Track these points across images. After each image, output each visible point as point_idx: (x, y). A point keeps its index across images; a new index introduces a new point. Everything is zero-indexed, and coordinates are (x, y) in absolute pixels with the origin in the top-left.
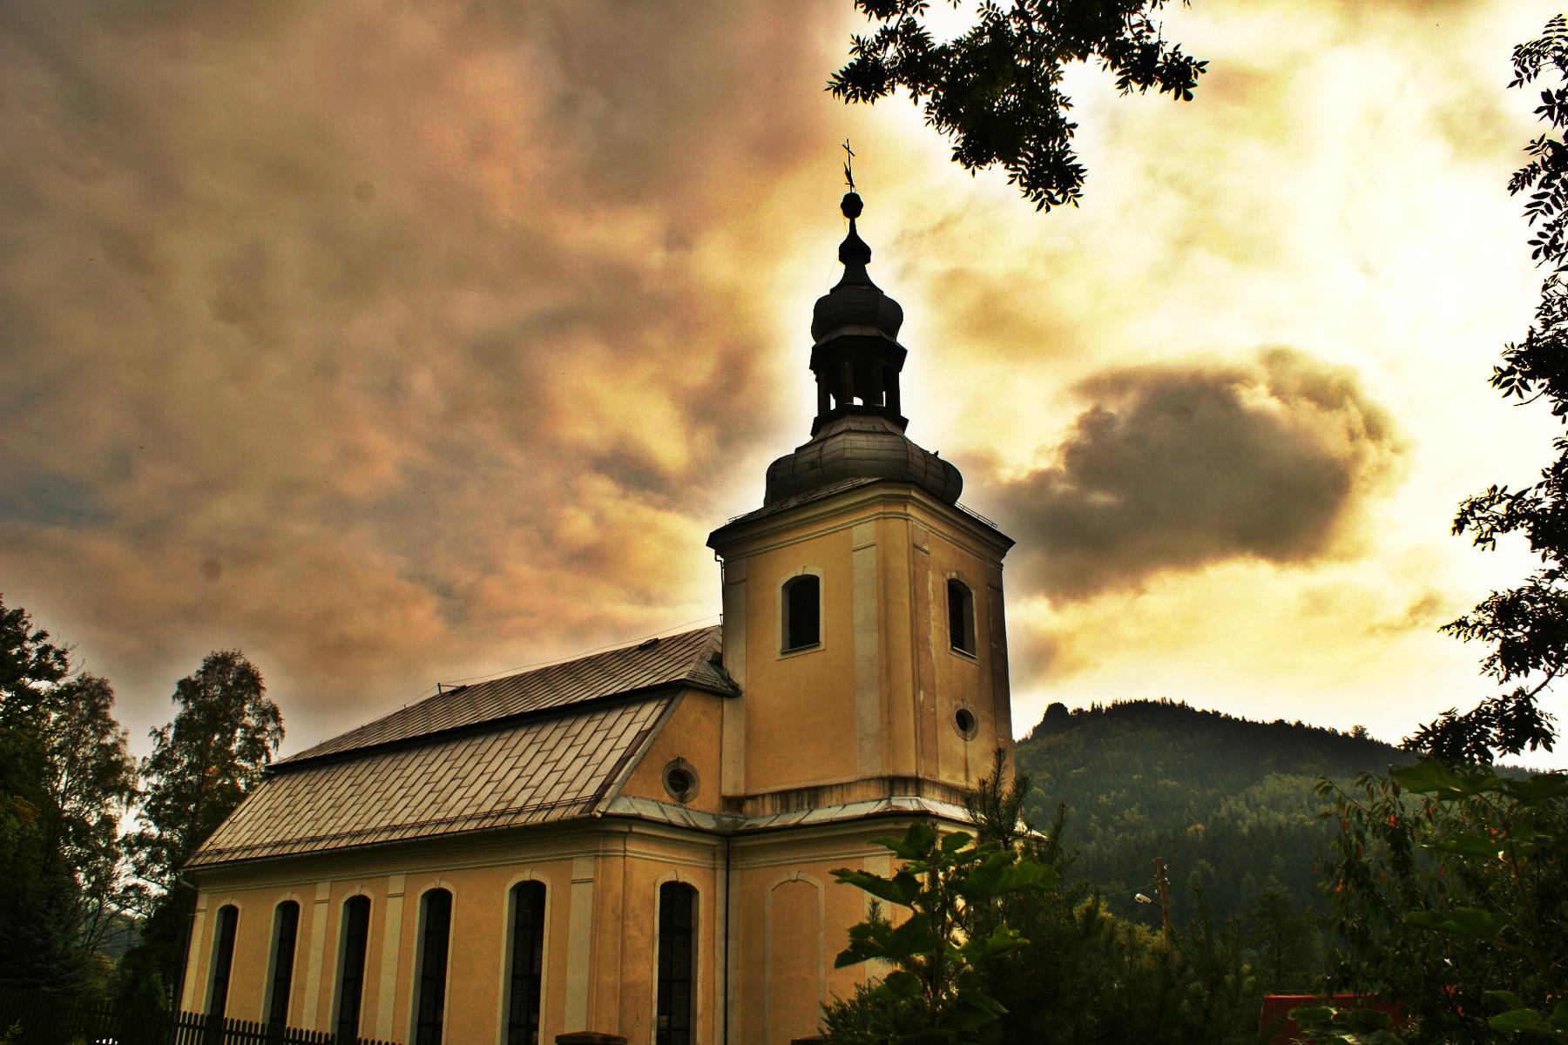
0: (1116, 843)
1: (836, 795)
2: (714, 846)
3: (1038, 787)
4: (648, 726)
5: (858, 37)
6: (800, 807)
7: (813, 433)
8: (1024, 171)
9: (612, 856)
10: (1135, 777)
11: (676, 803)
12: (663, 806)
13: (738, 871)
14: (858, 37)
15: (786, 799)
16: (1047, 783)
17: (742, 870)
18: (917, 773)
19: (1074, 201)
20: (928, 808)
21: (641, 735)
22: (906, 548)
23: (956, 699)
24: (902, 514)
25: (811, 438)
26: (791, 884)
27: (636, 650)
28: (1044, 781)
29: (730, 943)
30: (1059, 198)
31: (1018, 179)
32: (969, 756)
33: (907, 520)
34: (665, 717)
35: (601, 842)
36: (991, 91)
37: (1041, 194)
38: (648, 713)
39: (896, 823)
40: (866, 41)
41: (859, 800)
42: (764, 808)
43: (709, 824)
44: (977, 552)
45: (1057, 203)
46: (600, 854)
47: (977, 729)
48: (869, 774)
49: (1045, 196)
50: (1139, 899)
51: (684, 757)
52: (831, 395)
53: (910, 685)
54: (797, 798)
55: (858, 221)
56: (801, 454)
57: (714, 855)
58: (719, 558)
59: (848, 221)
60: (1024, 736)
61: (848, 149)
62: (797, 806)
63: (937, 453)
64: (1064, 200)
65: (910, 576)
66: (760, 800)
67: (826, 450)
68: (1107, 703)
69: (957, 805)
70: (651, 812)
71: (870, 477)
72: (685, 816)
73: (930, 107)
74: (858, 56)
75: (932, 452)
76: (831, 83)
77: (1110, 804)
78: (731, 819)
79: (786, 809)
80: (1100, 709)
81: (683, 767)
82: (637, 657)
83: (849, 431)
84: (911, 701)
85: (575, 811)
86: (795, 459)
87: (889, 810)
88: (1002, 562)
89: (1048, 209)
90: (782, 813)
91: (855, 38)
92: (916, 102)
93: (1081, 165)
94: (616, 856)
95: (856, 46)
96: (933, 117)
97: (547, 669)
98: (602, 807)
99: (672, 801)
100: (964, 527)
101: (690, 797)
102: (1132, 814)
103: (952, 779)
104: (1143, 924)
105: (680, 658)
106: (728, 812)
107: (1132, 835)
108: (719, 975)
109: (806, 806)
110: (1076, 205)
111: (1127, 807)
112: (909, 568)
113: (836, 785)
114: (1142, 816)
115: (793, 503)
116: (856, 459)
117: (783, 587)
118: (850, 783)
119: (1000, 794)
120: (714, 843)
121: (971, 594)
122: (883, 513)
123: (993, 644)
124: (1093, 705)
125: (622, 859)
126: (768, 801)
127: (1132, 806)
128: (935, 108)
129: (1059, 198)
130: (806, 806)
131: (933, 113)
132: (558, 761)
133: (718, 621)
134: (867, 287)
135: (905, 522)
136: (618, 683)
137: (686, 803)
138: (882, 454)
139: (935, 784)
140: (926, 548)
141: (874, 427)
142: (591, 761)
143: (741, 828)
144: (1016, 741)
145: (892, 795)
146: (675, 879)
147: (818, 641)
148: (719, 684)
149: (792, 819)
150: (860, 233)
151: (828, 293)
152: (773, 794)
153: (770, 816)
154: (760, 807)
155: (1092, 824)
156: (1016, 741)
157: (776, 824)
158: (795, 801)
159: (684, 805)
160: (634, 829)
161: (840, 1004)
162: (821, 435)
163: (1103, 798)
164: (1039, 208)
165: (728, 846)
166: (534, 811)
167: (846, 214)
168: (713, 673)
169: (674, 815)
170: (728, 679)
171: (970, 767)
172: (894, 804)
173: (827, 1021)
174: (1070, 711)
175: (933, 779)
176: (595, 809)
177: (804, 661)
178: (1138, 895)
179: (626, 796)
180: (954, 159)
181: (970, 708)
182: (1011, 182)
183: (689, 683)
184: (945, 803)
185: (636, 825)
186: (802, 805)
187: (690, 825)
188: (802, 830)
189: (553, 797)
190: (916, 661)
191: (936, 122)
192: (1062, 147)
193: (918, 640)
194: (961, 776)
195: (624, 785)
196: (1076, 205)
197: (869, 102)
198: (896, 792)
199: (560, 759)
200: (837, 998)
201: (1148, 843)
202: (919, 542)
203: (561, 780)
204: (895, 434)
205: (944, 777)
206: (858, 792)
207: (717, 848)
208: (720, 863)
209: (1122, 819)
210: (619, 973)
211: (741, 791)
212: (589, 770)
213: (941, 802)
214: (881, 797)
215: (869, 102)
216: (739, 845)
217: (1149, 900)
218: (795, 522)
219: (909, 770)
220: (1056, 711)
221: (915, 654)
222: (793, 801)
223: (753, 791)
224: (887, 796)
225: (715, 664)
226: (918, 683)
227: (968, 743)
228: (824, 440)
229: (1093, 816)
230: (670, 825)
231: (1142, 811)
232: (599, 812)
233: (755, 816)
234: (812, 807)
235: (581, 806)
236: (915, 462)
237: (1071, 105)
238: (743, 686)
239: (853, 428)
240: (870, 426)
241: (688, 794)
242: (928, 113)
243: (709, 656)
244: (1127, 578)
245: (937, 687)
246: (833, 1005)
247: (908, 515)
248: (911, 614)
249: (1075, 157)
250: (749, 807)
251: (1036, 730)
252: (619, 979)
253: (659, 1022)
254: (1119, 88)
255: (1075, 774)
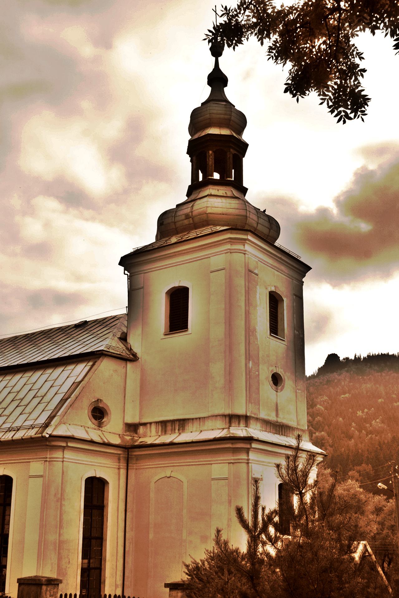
0: (366, 441)
1: (196, 424)
2: (120, 454)
3: (321, 405)
4: (79, 379)
5: (226, 7)
6: (173, 431)
7: (188, 195)
8: (330, 97)
9: (55, 461)
10: (380, 400)
11: (96, 427)
12: (87, 429)
13: (134, 470)
14: (226, 7)
15: (164, 425)
16: (325, 403)
17: (136, 469)
18: (246, 412)
19: (362, 118)
20: (253, 435)
21: (75, 385)
22: (244, 272)
23: (272, 366)
24: (242, 250)
25: (187, 198)
26: (167, 479)
27: (73, 328)
28: (323, 401)
29: (128, 514)
30: (352, 115)
31: (326, 102)
32: (278, 402)
33: (245, 254)
34: (90, 373)
35: (48, 452)
36: (311, 42)
37: (340, 112)
38: (81, 369)
39: (232, 444)
40: (231, 9)
41: (211, 428)
42: (151, 431)
43: (116, 441)
44: (288, 274)
45: (350, 119)
46: (48, 459)
47: (284, 384)
48: (216, 412)
49: (343, 114)
50: (380, 486)
51: (101, 399)
52: (200, 171)
53: (243, 357)
54: (172, 426)
55: (220, 58)
56: (180, 209)
57: (119, 459)
58: (126, 272)
59: (214, 58)
60: (312, 373)
61: (216, 12)
62: (172, 430)
63: (265, 211)
64: (355, 117)
65: (245, 290)
66: (148, 425)
67: (195, 208)
68: (364, 355)
69: (270, 432)
70: (80, 433)
71: (223, 226)
72: (102, 436)
73: (270, 48)
74: (225, 18)
75: (262, 210)
76: (207, 35)
77: (364, 417)
78: (130, 437)
79: (165, 432)
80: (359, 358)
81: (101, 405)
82: (74, 332)
83: (211, 195)
84: (244, 369)
85: (32, 433)
86: (176, 212)
87: (228, 435)
88: (303, 280)
89: (344, 122)
90: (162, 435)
91: (224, 7)
92: (262, 44)
93: (367, 96)
94: (57, 461)
95: (224, 12)
96: (273, 54)
97: (16, 337)
98: (49, 431)
99: (93, 426)
100: (280, 258)
101: (105, 423)
102: (377, 423)
103: (268, 416)
104: (382, 495)
105: (101, 335)
106: (128, 433)
107: (376, 436)
108: (121, 534)
109: (177, 431)
110: (363, 120)
111: (374, 419)
112: (245, 284)
113: (196, 419)
114: (383, 425)
115: (174, 240)
116: (214, 214)
117: (166, 293)
118: (204, 418)
119: (298, 463)
120: (119, 452)
121: (283, 300)
122: (230, 249)
123: (295, 331)
124: (355, 355)
125: (61, 463)
126: (153, 427)
127: (377, 419)
128: (274, 49)
129: (352, 115)
130: (177, 431)
131: (273, 53)
132: (22, 399)
133: (124, 311)
134: (224, 103)
135: (244, 255)
136: (61, 350)
137: (101, 427)
138: (231, 211)
139: (257, 419)
140: (256, 271)
141: (226, 193)
142: (43, 400)
143: (136, 444)
144: (308, 376)
145: (230, 426)
146: (95, 476)
147: (187, 328)
148: (125, 353)
149: (167, 439)
150: (221, 67)
151: (200, 105)
152: (157, 423)
153: (155, 436)
154: (149, 432)
155: (353, 429)
156: (308, 376)
157: (157, 442)
158: (170, 428)
159: (100, 429)
160: (70, 444)
161: (195, 562)
162: (193, 197)
163: (359, 413)
164: (339, 121)
165: (128, 454)
166: (7, 431)
167: (213, 54)
168: (121, 346)
169: (95, 436)
170: (130, 350)
171: (279, 408)
172: (231, 432)
173: (187, 574)
174: (341, 359)
175: (256, 416)
176: (45, 431)
177: (179, 338)
178: (380, 484)
179: (64, 423)
180: (286, 91)
181: (280, 371)
182: (321, 104)
183: (106, 353)
184: (263, 431)
185: (70, 441)
186: (175, 430)
187: (104, 442)
188: (174, 446)
189: (18, 424)
190: (248, 343)
191: (274, 58)
192: (356, 83)
193: (249, 329)
194: (274, 414)
195: (64, 416)
196: (363, 120)
197: (232, 48)
198: (233, 425)
199: (23, 398)
200: (194, 559)
201: (386, 441)
202: (251, 267)
203: (23, 412)
204: (239, 199)
205: (263, 415)
206: (209, 424)
207: (121, 456)
208: (123, 465)
209: (371, 426)
210: (58, 534)
211: (136, 420)
212: (41, 406)
213: (260, 430)
214: (224, 427)
215: (232, 48)
216: (135, 454)
217: (386, 487)
218: (175, 252)
219: (241, 411)
220: (332, 359)
221: (247, 337)
222: (169, 427)
223: (144, 421)
224: (227, 426)
225: (121, 339)
226: (248, 357)
227: (278, 393)
228: (195, 200)
229: (353, 424)
230: (92, 442)
231: (383, 422)
232: (47, 434)
233: (145, 436)
234: (181, 431)
235: (37, 429)
236: (251, 217)
237: (363, 58)
238: (139, 355)
239: (213, 194)
240: (224, 192)
241: (103, 422)
242: (269, 52)
243: (119, 335)
244: (388, 364)
245: (260, 359)
246: (190, 563)
247: (245, 251)
248: (246, 313)
249: (363, 90)
250: (141, 430)
251: (320, 370)
252: (58, 539)
253: (82, 563)
254: (395, 49)
255: (343, 398)
